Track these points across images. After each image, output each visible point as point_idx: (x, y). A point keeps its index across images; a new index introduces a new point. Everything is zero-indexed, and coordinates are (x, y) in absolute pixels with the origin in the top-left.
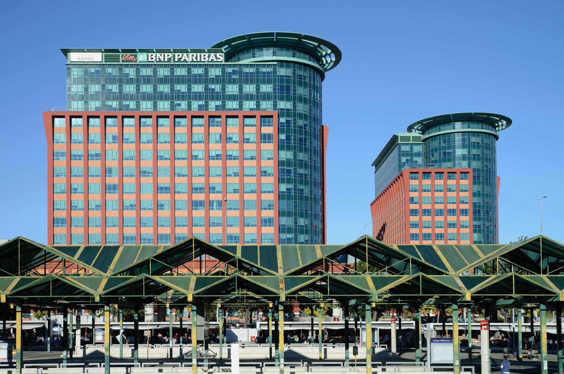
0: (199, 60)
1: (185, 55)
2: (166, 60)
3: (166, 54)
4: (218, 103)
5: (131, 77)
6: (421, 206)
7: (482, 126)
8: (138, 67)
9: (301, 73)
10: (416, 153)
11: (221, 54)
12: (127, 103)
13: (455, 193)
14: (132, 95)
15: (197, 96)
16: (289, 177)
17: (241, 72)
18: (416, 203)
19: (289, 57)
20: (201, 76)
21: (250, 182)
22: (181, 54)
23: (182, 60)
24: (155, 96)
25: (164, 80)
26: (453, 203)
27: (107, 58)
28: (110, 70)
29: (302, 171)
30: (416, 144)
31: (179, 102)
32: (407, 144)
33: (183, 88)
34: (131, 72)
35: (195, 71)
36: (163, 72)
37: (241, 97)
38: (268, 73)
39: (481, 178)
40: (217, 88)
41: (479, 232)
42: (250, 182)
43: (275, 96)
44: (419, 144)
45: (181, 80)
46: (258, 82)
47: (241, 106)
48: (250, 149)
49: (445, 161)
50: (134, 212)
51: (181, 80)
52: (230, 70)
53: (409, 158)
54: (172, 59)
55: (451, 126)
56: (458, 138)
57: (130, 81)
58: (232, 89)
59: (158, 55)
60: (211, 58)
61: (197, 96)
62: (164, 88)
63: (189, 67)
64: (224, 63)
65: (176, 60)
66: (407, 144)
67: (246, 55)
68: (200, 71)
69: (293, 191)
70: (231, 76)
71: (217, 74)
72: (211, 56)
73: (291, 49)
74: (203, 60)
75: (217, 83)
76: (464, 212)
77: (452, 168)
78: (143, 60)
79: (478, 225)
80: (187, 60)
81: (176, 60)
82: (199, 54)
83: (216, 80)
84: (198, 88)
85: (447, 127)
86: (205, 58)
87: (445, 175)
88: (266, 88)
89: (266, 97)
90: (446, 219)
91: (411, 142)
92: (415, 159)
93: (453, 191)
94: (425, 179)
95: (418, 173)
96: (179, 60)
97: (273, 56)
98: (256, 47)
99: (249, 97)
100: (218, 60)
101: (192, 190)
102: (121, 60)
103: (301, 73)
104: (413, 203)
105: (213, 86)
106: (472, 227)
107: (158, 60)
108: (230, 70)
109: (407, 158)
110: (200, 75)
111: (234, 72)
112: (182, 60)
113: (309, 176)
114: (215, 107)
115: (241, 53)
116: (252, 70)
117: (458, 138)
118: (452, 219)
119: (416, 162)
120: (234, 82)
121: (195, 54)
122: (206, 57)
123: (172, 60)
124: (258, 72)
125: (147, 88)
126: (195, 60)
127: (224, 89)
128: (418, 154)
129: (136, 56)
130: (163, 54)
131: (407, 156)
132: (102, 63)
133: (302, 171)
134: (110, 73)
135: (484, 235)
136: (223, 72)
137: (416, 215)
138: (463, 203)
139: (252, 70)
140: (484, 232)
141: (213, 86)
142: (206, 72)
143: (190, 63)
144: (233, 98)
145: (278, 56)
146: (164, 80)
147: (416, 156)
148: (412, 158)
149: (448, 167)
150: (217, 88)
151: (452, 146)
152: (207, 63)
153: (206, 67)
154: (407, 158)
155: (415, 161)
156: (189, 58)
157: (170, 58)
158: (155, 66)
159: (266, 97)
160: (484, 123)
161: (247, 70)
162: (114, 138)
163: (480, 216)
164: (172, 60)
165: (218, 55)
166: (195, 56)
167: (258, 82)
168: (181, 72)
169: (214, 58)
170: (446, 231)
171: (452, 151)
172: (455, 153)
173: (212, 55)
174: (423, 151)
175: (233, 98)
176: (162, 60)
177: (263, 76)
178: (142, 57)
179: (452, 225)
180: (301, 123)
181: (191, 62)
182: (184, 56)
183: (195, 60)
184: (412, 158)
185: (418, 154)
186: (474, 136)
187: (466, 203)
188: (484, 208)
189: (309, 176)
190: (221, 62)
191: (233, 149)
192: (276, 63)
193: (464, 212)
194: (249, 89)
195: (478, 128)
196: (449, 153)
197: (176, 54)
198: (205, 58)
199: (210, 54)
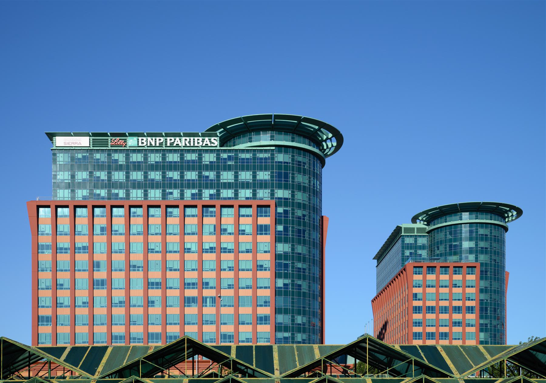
0: (192, 145)
1: (178, 139)
2: (158, 145)
3: (158, 138)
4: (213, 191)
5: (120, 163)
6: (424, 303)
7: (491, 217)
8: (128, 152)
9: (300, 159)
10: (420, 246)
11: (216, 138)
12: (116, 191)
13: (461, 289)
14: (121, 183)
15: (191, 184)
16: (286, 271)
17: (236, 158)
18: (419, 300)
19: (487, 220)
20: (194, 162)
21: (246, 277)
22: (173, 138)
23: (175, 145)
24: (146, 184)
25: (155, 167)
26: (459, 300)
27: (95, 143)
28: (98, 156)
29: (300, 265)
30: (420, 236)
31: (171, 191)
32: (411, 236)
33: (175, 175)
34: (120, 158)
35: (189, 157)
36: (154, 158)
37: (237, 185)
38: (266, 159)
39: (488, 273)
40: (212, 175)
41: (486, 331)
42: (246, 277)
43: (273, 184)
44: (424, 236)
45: (173, 166)
46: (254, 169)
47: (236, 194)
48: (246, 241)
49: (450, 255)
50: (123, 309)
51: (173, 166)
52: (225, 156)
53: (413, 251)
54: (164, 143)
55: (458, 217)
56: (465, 230)
57: (120, 168)
58: (227, 176)
59: (149, 139)
60: (205, 143)
61: (191, 184)
62: (156, 176)
63: (182, 152)
64: (218, 148)
65: (168, 145)
66: (411, 236)
67: (242, 139)
68: (193, 157)
69: (290, 287)
70: (226, 163)
71: (212, 160)
72: (205, 141)
73: (290, 133)
74: (196, 144)
75: (211, 170)
76: (470, 310)
77: (458, 262)
78: (133, 145)
79: (485, 324)
80: (180, 145)
81: (168, 145)
82: (192, 138)
83: (211, 167)
84: (192, 175)
85: (453, 218)
86: (199, 142)
87: (451, 269)
88: (263, 175)
89: (263, 185)
90: (451, 317)
91: (416, 234)
92: (420, 252)
93: (459, 287)
94: (430, 274)
95: (422, 267)
96: (172, 144)
97: (476, 219)
98: (253, 131)
99: (245, 185)
100: (212, 145)
101: (185, 285)
102: (109, 145)
103: (300, 159)
104: (416, 300)
105: (206, 173)
106: (478, 325)
107: (149, 145)
108: (225, 156)
109: (411, 251)
110: (193, 161)
111: (230, 158)
112: (175, 145)
113: (307, 271)
114: (208, 196)
115: (448, 215)
116: (248, 156)
117: (465, 230)
118: (457, 317)
119: (421, 255)
120: (228, 168)
121: (188, 139)
122: (200, 141)
123: (164, 145)
124: (254, 158)
125: (137, 176)
126: (188, 145)
127: (218, 176)
128: (423, 247)
129: (125, 141)
130: (154, 138)
131: (411, 249)
132: (89, 148)
133: (300, 265)
134: (98, 159)
135: (491, 334)
136: (218, 158)
137: (419, 313)
138: (469, 300)
139: (248, 156)
140: (491, 331)
141: (206, 173)
142: (200, 158)
143: (183, 148)
144: (227, 186)
145: (479, 219)
146: (155, 167)
147: (420, 249)
148: (416, 251)
149: (454, 261)
150: (212, 175)
151: (458, 238)
152: (201, 148)
153: (200, 152)
154: (411, 251)
155: (420, 254)
156: (181, 142)
157: (162, 143)
158: (145, 152)
159: (263, 185)
160: (493, 214)
161: (243, 156)
162: (102, 229)
163: (487, 313)
164: (164, 145)
165: (212, 139)
166: (188, 140)
167: (254, 169)
168: (173, 158)
169: (208, 143)
170: (451, 329)
171: (458, 243)
172: (461, 245)
173: (207, 139)
174: (427, 244)
175: (227, 186)
176: (154, 145)
177: (260, 162)
178: (132, 142)
179: (457, 324)
180: (299, 213)
181: (184, 147)
182: (176, 141)
183: (188, 145)
184: (416, 251)
185: (423, 247)
186: (482, 227)
187: (472, 300)
188: (491, 305)
189: (307, 271)
190: (216, 147)
191: (228, 241)
192: (273, 148)
193: (470, 310)
194: (245, 176)
195: (487, 219)
196: (455, 246)
197: (168, 139)
198: (199, 142)
199: (175, 138)
